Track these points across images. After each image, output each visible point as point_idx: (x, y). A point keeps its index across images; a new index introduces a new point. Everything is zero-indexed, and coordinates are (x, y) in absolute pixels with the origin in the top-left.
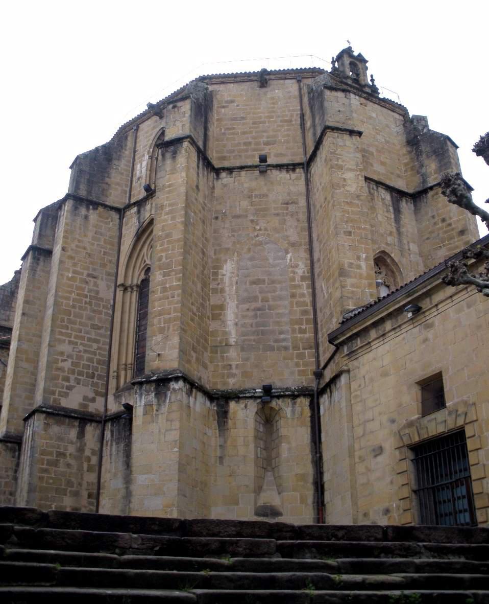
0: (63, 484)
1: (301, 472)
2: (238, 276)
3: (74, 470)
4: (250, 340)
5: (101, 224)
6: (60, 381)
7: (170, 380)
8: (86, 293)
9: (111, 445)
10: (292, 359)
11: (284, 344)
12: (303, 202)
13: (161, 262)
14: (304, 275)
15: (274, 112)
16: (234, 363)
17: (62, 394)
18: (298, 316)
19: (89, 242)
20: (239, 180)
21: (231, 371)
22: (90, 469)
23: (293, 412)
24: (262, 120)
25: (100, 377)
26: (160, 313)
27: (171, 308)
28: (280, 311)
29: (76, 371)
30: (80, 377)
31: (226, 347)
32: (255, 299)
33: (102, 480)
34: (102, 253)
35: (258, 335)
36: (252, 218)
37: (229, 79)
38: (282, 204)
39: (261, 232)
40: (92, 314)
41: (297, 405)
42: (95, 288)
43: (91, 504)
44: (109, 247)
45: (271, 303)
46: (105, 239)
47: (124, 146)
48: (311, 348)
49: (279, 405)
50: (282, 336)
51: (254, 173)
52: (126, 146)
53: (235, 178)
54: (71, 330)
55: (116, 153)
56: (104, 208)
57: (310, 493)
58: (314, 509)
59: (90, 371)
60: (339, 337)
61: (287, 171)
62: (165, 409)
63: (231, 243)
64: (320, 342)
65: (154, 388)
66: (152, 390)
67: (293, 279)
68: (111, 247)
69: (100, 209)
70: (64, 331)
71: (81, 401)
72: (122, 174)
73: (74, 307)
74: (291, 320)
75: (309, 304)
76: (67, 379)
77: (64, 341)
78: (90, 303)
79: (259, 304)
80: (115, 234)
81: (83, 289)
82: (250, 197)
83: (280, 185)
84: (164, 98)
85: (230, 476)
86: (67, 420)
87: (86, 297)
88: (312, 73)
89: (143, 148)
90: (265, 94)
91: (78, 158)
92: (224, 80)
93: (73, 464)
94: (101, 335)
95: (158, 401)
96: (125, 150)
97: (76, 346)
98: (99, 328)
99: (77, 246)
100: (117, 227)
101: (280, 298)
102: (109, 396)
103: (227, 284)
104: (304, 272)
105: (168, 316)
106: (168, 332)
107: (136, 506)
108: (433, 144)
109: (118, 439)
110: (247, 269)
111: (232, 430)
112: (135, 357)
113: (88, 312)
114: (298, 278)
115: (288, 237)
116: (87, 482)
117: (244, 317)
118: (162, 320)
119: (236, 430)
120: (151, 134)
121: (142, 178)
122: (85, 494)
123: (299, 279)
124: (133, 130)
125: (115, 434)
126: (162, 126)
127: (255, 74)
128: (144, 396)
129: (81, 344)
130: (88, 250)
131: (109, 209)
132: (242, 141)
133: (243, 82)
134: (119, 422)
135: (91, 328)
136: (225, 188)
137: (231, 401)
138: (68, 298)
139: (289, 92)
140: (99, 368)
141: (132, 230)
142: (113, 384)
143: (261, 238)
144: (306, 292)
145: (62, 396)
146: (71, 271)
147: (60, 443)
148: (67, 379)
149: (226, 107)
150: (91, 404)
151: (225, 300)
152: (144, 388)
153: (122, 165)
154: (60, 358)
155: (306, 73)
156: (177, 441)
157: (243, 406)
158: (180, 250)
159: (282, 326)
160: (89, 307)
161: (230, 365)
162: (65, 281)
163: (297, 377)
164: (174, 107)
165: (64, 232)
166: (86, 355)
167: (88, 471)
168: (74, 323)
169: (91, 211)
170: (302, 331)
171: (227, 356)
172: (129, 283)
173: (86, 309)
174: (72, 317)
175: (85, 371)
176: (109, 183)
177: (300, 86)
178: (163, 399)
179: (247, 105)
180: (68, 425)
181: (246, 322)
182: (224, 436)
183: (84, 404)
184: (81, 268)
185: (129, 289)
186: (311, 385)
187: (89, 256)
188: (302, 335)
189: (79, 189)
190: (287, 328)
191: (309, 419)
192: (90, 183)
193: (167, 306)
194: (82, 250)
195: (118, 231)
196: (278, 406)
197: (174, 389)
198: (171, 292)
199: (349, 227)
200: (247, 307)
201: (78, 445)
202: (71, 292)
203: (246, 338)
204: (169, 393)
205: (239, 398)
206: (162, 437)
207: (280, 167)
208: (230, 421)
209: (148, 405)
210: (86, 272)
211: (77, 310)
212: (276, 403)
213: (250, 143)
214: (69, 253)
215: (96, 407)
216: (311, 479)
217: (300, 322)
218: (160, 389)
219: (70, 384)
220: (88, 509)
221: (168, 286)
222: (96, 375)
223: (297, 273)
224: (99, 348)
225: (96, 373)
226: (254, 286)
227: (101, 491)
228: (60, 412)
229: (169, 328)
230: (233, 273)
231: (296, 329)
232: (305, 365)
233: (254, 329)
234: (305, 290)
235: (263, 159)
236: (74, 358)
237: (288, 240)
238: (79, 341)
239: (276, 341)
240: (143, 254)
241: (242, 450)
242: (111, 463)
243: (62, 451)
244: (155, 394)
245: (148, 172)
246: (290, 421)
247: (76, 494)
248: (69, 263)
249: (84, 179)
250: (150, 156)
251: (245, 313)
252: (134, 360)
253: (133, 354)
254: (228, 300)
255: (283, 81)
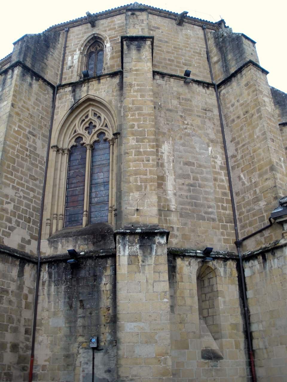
0: (5, 321)
1: (234, 322)
2: (174, 156)
3: (15, 307)
4: (187, 209)
5: (41, 94)
6: (4, 221)
7: (156, 234)
8: (27, 147)
9: (49, 285)
10: (218, 229)
11: (212, 216)
12: (216, 112)
13: (134, 129)
14: (221, 165)
15: (188, 44)
16: (175, 226)
17: (5, 234)
18: (220, 196)
19: (32, 105)
20: (169, 84)
21: (173, 233)
22: (27, 307)
23: (225, 272)
24: (181, 47)
25: (34, 223)
26: (136, 173)
27: (146, 170)
28: (207, 190)
29: (17, 214)
30: (19, 220)
31: (168, 212)
32: (187, 177)
33: (38, 318)
34: (40, 117)
35: (192, 206)
36: (181, 114)
37: (156, 12)
38: (202, 110)
39: (189, 126)
40: (30, 166)
41: (228, 267)
42: (34, 145)
43: (27, 339)
44: (45, 113)
45: (200, 182)
46: (42, 107)
47: (57, 40)
48: (231, 222)
49: (214, 265)
50: (210, 210)
51: (180, 82)
52: (59, 40)
53: (166, 81)
54: (15, 177)
55: (52, 44)
56: (43, 82)
57: (241, 339)
58: (246, 354)
59: (28, 216)
60: (284, 216)
61: (203, 87)
62: (151, 261)
63: (167, 130)
64: (237, 219)
65: (138, 240)
66: (137, 241)
67: (214, 167)
68: (46, 114)
69: (41, 82)
70: (9, 176)
71: (20, 242)
72: (56, 60)
73: (17, 156)
74: (215, 198)
75: (227, 188)
76: (10, 221)
77: (9, 185)
78: (30, 156)
79: (191, 181)
80: (49, 105)
81: (25, 143)
82: (179, 98)
83: (199, 96)
84: (60, 24)
85: (181, 323)
86: (10, 259)
87: (27, 150)
88: (213, 26)
89: (74, 45)
90: (181, 30)
91: (26, 36)
92: (151, 11)
93: (14, 301)
94: (36, 185)
95: (144, 252)
96: (58, 43)
97: (18, 192)
98: (36, 179)
99: (22, 106)
100: (51, 100)
101: (206, 180)
102: (41, 241)
103: (166, 161)
104: (221, 163)
105: (145, 177)
106: (145, 191)
107: (125, 353)
108: (277, 98)
109: (58, 280)
110: (180, 152)
111: (180, 283)
112: (65, 209)
113: (28, 164)
114: (217, 167)
115: (208, 134)
116: (25, 319)
117: (180, 189)
118: (138, 179)
119: (183, 283)
120: (83, 37)
121: (74, 67)
122: (23, 330)
123: (219, 168)
124: (64, 31)
125: (53, 276)
126: (94, 33)
127: (176, 15)
128: (127, 247)
129: (22, 190)
130: (30, 112)
131: (46, 83)
132: (167, 58)
133: (165, 17)
134: (58, 265)
135: (29, 178)
136: (160, 87)
137: (178, 258)
138: (13, 148)
139: (197, 34)
140: (34, 214)
141: (66, 104)
142: (46, 231)
143: (188, 131)
144: (224, 178)
145: (5, 236)
146: (17, 125)
147: (4, 280)
148: (10, 221)
149: (155, 31)
150: (27, 246)
151: (165, 173)
152: (127, 239)
153: (55, 54)
154: (5, 200)
155: (209, 25)
156: (166, 292)
157: (187, 263)
158: (151, 123)
159: (209, 202)
160: (29, 159)
161: (173, 228)
162: (12, 132)
163: (223, 244)
164: (133, 14)
165: (13, 92)
166: (25, 201)
167: (25, 308)
168: (17, 171)
169: (34, 81)
170: (224, 208)
171: (169, 219)
172: (64, 148)
173: (26, 161)
174: (15, 165)
175: (24, 215)
176: (47, 64)
177: (204, 32)
178: (149, 251)
179: (169, 34)
180: (11, 263)
181: (182, 193)
182: (174, 288)
183: (22, 245)
184: (24, 125)
185: (61, 152)
186: (233, 251)
187: (31, 116)
188: (224, 211)
189: (26, 61)
190: (212, 204)
191: (237, 279)
192: (34, 59)
193: (142, 168)
194: (26, 110)
195: (51, 103)
196: (214, 266)
197: (159, 243)
198: (145, 156)
199: (272, 136)
200: (183, 182)
201: (19, 282)
202: (16, 144)
203: (183, 207)
204: (155, 247)
205: (184, 256)
206: (150, 287)
207: (198, 82)
208: (177, 275)
209: (133, 256)
210: (28, 130)
211: (20, 160)
212: (212, 263)
213: (173, 61)
214: (17, 110)
215: (30, 249)
216: (241, 328)
217: (222, 201)
218: (144, 241)
219: (12, 225)
220: (24, 344)
221: (142, 150)
222: (32, 220)
223: (217, 163)
224: (34, 197)
225: (32, 218)
226: (187, 166)
227: (37, 328)
228: (6, 251)
229: (146, 187)
230: (170, 153)
231: (219, 205)
232: (228, 235)
233: (189, 200)
234: (223, 177)
235: (187, 74)
236: (16, 202)
237: (209, 137)
238: (21, 188)
239: (206, 213)
240: (75, 123)
241: (189, 301)
242: (49, 302)
243: (5, 288)
244: (140, 246)
245: (80, 64)
246: (223, 279)
247: (15, 330)
248: (16, 119)
249: (30, 54)
250: (81, 52)
251: (181, 187)
252: (65, 212)
253: (64, 206)
254: (167, 174)
255: (192, 26)
